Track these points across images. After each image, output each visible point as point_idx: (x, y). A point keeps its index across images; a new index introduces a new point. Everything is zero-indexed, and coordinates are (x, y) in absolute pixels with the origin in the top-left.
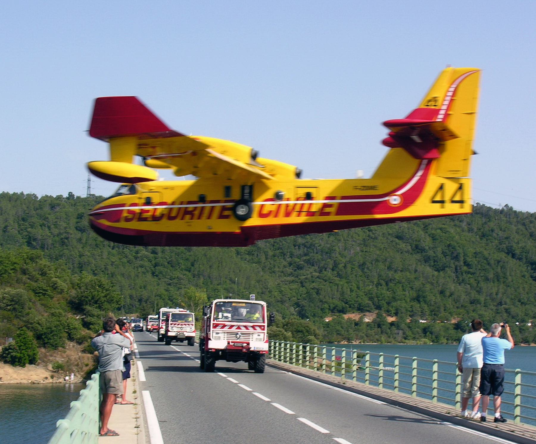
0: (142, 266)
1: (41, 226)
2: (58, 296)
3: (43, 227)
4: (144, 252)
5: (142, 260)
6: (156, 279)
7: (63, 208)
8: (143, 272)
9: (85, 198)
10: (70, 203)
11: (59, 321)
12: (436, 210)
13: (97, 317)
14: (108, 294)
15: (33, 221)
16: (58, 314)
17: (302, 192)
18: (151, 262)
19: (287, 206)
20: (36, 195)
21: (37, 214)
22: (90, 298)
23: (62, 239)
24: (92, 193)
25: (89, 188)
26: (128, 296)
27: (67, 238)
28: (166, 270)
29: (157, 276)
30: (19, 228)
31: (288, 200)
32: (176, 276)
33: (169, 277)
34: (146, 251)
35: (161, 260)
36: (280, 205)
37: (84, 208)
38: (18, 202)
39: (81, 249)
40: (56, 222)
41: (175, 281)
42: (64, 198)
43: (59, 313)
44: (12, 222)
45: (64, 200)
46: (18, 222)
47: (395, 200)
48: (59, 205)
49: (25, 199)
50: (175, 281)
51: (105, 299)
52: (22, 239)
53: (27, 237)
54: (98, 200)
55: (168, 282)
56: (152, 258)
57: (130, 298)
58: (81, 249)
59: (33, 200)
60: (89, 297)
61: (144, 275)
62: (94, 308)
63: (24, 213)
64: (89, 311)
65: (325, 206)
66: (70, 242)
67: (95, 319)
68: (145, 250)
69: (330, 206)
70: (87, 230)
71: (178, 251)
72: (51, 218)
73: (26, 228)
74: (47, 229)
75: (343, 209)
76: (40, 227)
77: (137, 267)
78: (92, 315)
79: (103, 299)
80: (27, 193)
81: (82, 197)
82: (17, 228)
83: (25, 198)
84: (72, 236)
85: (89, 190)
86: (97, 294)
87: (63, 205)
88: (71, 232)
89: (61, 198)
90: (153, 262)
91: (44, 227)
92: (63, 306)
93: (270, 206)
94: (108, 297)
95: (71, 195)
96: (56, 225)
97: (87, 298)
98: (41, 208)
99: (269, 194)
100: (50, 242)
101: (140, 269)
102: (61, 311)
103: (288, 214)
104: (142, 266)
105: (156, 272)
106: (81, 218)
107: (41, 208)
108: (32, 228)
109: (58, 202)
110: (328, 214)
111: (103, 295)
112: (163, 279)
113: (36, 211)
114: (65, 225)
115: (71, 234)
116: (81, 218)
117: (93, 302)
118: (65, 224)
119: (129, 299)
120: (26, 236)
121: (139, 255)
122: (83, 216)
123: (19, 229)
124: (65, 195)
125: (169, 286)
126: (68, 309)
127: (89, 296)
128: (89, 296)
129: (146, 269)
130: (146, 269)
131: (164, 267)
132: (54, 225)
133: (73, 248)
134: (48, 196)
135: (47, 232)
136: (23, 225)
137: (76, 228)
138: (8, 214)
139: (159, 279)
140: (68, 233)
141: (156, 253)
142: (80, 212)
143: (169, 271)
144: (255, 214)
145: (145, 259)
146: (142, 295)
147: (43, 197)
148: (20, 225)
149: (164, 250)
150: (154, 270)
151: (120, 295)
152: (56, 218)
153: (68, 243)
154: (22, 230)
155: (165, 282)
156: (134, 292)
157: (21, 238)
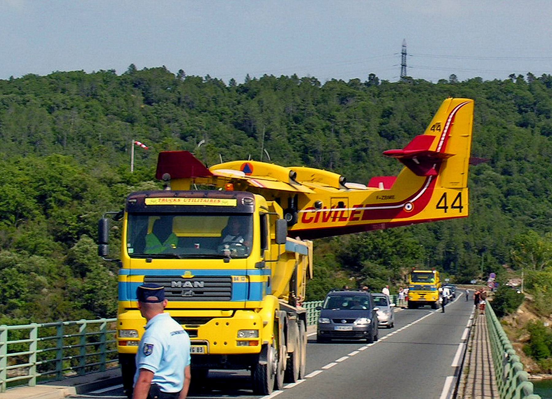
0: (485, 195)
1: (323, 130)
2: (323, 245)
3: (327, 132)
4: (489, 172)
5: (486, 184)
6: (509, 216)
7: (359, 100)
8: (487, 205)
9: (396, 84)
10: (371, 92)
11: (321, 284)
12: (440, 214)
13: (381, 278)
14: (399, 243)
15: (310, 122)
16: (320, 273)
17: (336, 202)
18: (501, 187)
19: (325, 213)
20: (316, 79)
21: (318, 111)
22: (370, 248)
23: (356, 151)
24: (408, 76)
25: (404, 66)
26: (462, 245)
27: (365, 150)
28: (524, 200)
29: (510, 211)
30: (289, 133)
31: (325, 208)
32: (542, 211)
33: (529, 213)
34: (493, 170)
35: (518, 184)
36: (319, 213)
37: (394, 100)
38: (289, 91)
39: (387, 168)
40: (348, 123)
41: (540, 219)
42: (361, 84)
43: (321, 271)
44: (278, 125)
45: (361, 87)
46: (287, 124)
47: (409, 207)
48: (353, 95)
49: (299, 86)
50: (540, 219)
51: (394, 250)
52: (294, 151)
53: (302, 148)
54: (416, 87)
55: (529, 222)
56: (503, 181)
57: (465, 247)
58: (387, 168)
59: (312, 87)
60: (368, 246)
61: (488, 210)
62: (376, 263)
63: (297, 109)
64: (368, 268)
65: (354, 212)
66: (370, 156)
67: (378, 281)
68: (491, 169)
69: (359, 212)
70: (398, 137)
71: (544, 169)
72: (341, 116)
73: (301, 133)
74: (333, 135)
75: (368, 215)
76: (321, 132)
77: (477, 197)
78: (374, 274)
79: (390, 250)
80: (304, 77)
81: (391, 81)
82: (286, 134)
83: (299, 84)
84: (373, 146)
85: (403, 70)
86: (382, 242)
87: (359, 96)
88: (371, 139)
89: (356, 84)
90: (505, 188)
91: (328, 132)
92: (330, 261)
93: (311, 213)
94: (398, 247)
95: (372, 78)
96: (347, 128)
97: (366, 248)
98: (325, 101)
99: (311, 204)
100: (338, 155)
101: (482, 200)
102: (325, 268)
103: (325, 220)
104: (485, 195)
105: (509, 205)
106: (388, 117)
107: (325, 101)
108: (310, 133)
109: (352, 90)
110: (357, 219)
111: (391, 243)
112: (520, 215)
113: (316, 105)
114: (361, 128)
115: (372, 143)
116: (388, 117)
117: (375, 255)
118: (363, 126)
119: (464, 250)
120: (300, 147)
121: (481, 176)
122: (391, 113)
123: (289, 136)
124: (364, 79)
125: (529, 228)
126: (336, 265)
127: (370, 245)
128: (370, 245)
129: (492, 199)
130: (492, 199)
131: (523, 197)
132: (345, 127)
133: (374, 165)
134: (336, 80)
135: (334, 140)
136: (295, 129)
137: (380, 133)
138: (272, 111)
139: (514, 216)
140: (366, 141)
141: (510, 174)
142: (386, 107)
143: (529, 202)
144: (299, 220)
145: (491, 183)
146: (483, 243)
147: (328, 83)
148: (291, 129)
149: (523, 168)
150: (505, 202)
151: (417, 244)
152: (348, 117)
153: (366, 158)
154: (294, 137)
155: (523, 221)
156: (471, 239)
157: (291, 149)
